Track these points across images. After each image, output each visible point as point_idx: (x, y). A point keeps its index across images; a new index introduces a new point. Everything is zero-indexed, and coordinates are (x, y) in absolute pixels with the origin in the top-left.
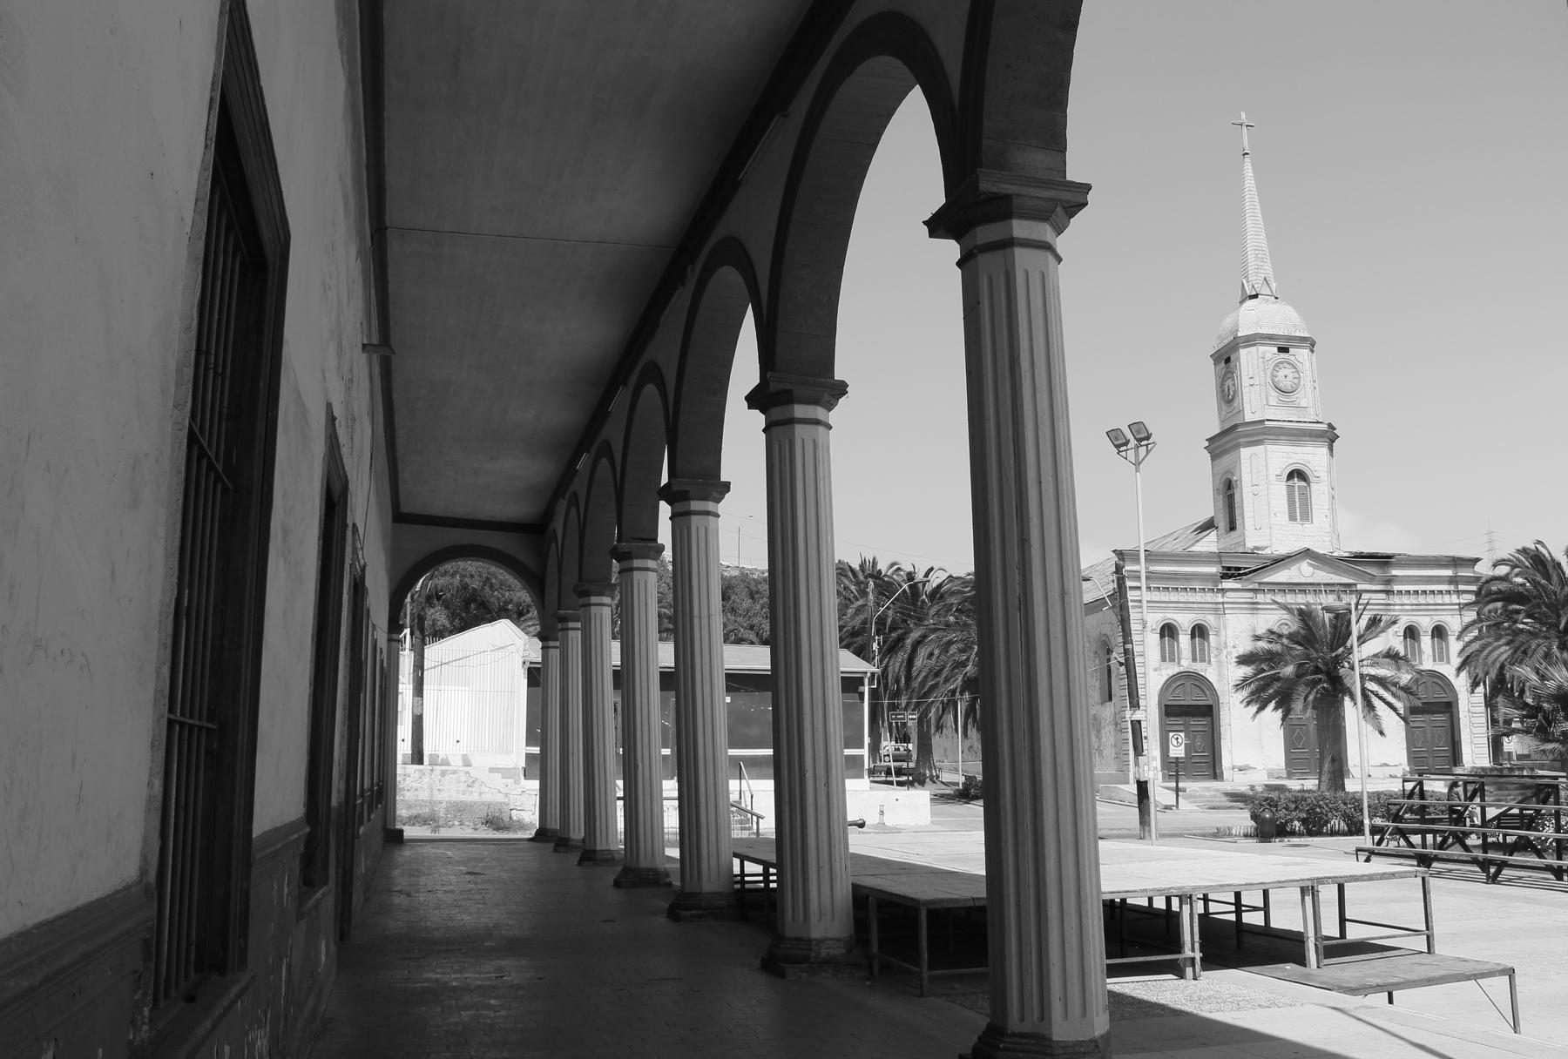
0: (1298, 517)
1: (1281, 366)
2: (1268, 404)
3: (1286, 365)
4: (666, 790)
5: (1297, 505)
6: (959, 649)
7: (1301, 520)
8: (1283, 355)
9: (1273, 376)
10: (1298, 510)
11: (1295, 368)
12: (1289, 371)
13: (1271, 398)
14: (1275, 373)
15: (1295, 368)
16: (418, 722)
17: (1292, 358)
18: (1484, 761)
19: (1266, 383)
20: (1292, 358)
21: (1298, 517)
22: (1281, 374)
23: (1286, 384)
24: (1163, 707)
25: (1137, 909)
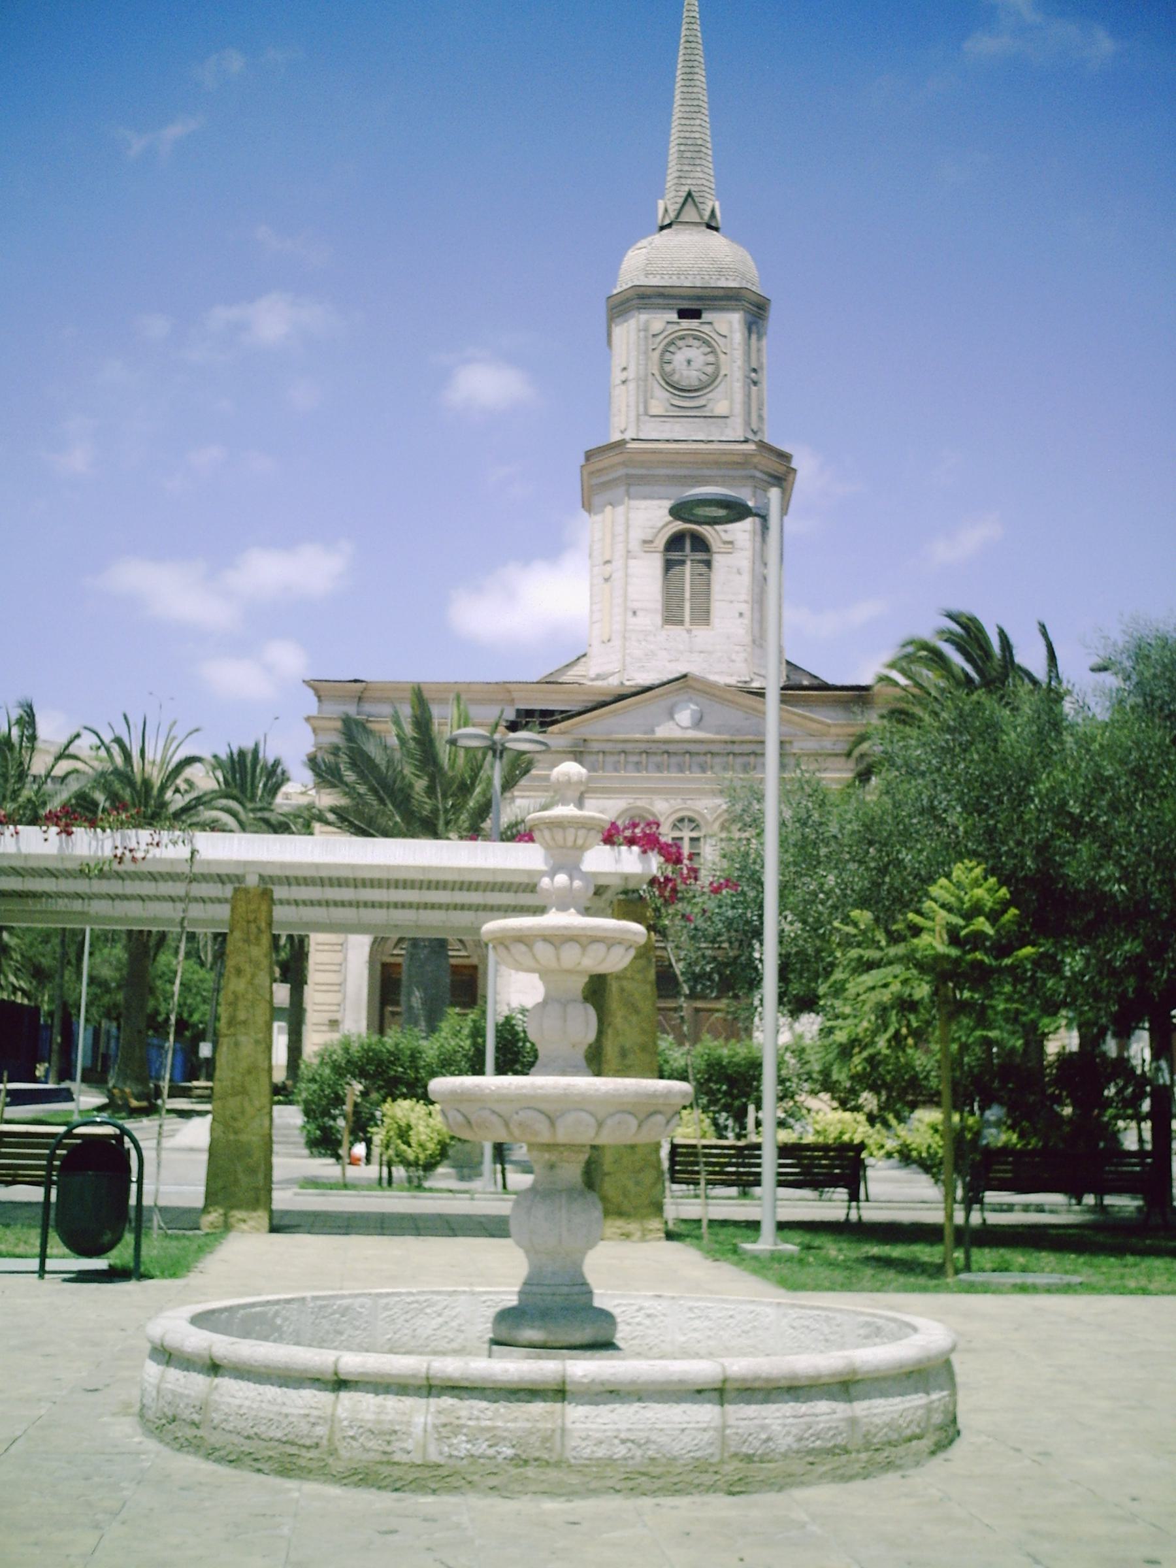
0: (687, 618)
1: (680, 343)
2: (646, 414)
3: (691, 341)
4: (563, 1410)
5: (687, 595)
6: (418, 1091)
7: (693, 621)
8: (686, 323)
9: (663, 362)
10: (687, 605)
11: (709, 345)
12: (696, 353)
13: (653, 402)
14: (668, 368)
15: (709, 345)
16: (330, 1005)
17: (706, 329)
18: (276, 896)
19: (646, 375)
20: (706, 329)
21: (687, 618)
22: (679, 358)
23: (690, 376)
24: (379, 967)
25: (1170, 1109)
